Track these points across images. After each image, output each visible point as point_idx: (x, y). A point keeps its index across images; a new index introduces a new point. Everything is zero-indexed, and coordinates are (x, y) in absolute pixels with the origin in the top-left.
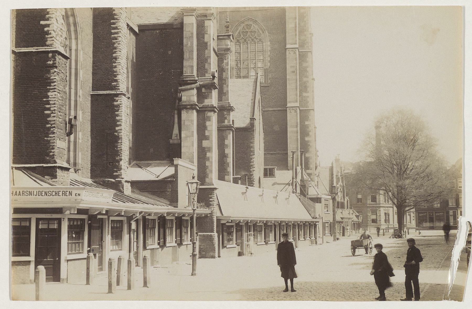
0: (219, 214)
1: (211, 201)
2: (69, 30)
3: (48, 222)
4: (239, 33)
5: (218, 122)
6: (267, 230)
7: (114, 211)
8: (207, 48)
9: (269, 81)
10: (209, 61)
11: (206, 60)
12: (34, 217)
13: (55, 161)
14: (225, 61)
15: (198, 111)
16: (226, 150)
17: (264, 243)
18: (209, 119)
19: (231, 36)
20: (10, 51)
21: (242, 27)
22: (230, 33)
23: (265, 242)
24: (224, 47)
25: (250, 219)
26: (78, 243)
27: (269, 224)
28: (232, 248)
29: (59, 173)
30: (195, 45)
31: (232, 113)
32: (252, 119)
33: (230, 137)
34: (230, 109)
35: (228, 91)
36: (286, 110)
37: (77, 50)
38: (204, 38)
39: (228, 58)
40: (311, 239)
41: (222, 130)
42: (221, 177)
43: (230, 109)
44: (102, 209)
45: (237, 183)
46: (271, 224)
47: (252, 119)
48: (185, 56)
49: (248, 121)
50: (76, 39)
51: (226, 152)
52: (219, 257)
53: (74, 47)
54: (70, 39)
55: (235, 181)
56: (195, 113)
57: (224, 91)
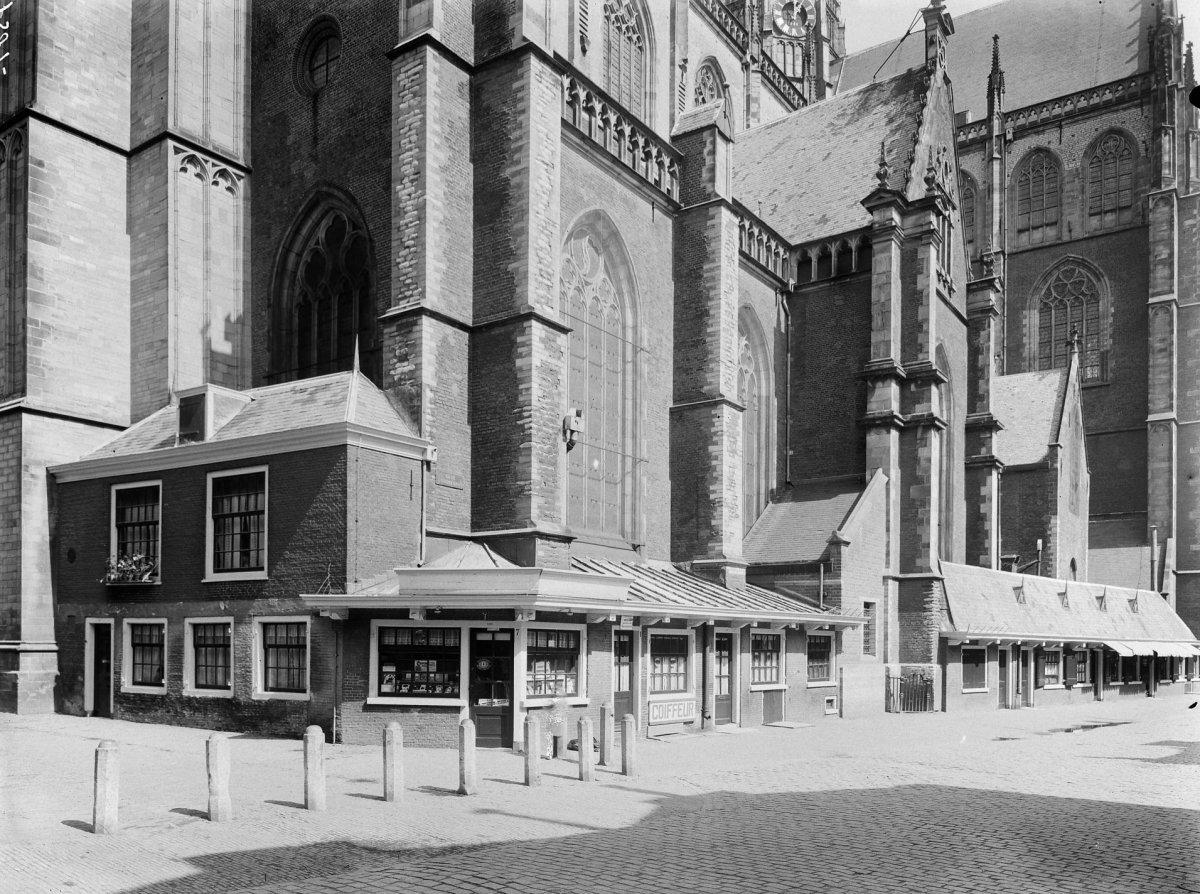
0: (945, 627)
1: (927, 602)
2: (620, 293)
3: (154, 645)
4: (1049, 289)
5: (968, 454)
6: (1041, 661)
7: (652, 616)
8: (922, 304)
9: (1111, 375)
10: (925, 328)
11: (920, 326)
12: (465, 626)
13: (532, 523)
14: (982, 333)
15: (900, 430)
16: (982, 506)
17: (1064, 686)
18: (925, 443)
19: (997, 281)
20: (931, 445)
21: (1055, 277)
22: (995, 276)
23: (1064, 683)
24: (982, 304)
25: (1021, 639)
26: (821, 666)
27: (1076, 649)
28: (93, 766)
29: (542, 549)
30: (897, 300)
31: (996, 437)
32: (1053, 448)
33: (994, 479)
34: (992, 426)
35: (988, 391)
36: (1146, 429)
37: (635, 328)
38: (915, 283)
39: (989, 326)
40: (1189, 680)
41: (978, 466)
42: (975, 554)
43: (992, 426)
44: (663, 616)
45: (1009, 569)
46: (1057, 649)
47: (1053, 448)
48: (874, 325)
49: (1044, 451)
50: (634, 305)
51: (982, 511)
52: (944, 709)
53: (630, 322)
54: (623, 308)
55: (1006, 566)
56: (894, 434)
57: (981, 392)
